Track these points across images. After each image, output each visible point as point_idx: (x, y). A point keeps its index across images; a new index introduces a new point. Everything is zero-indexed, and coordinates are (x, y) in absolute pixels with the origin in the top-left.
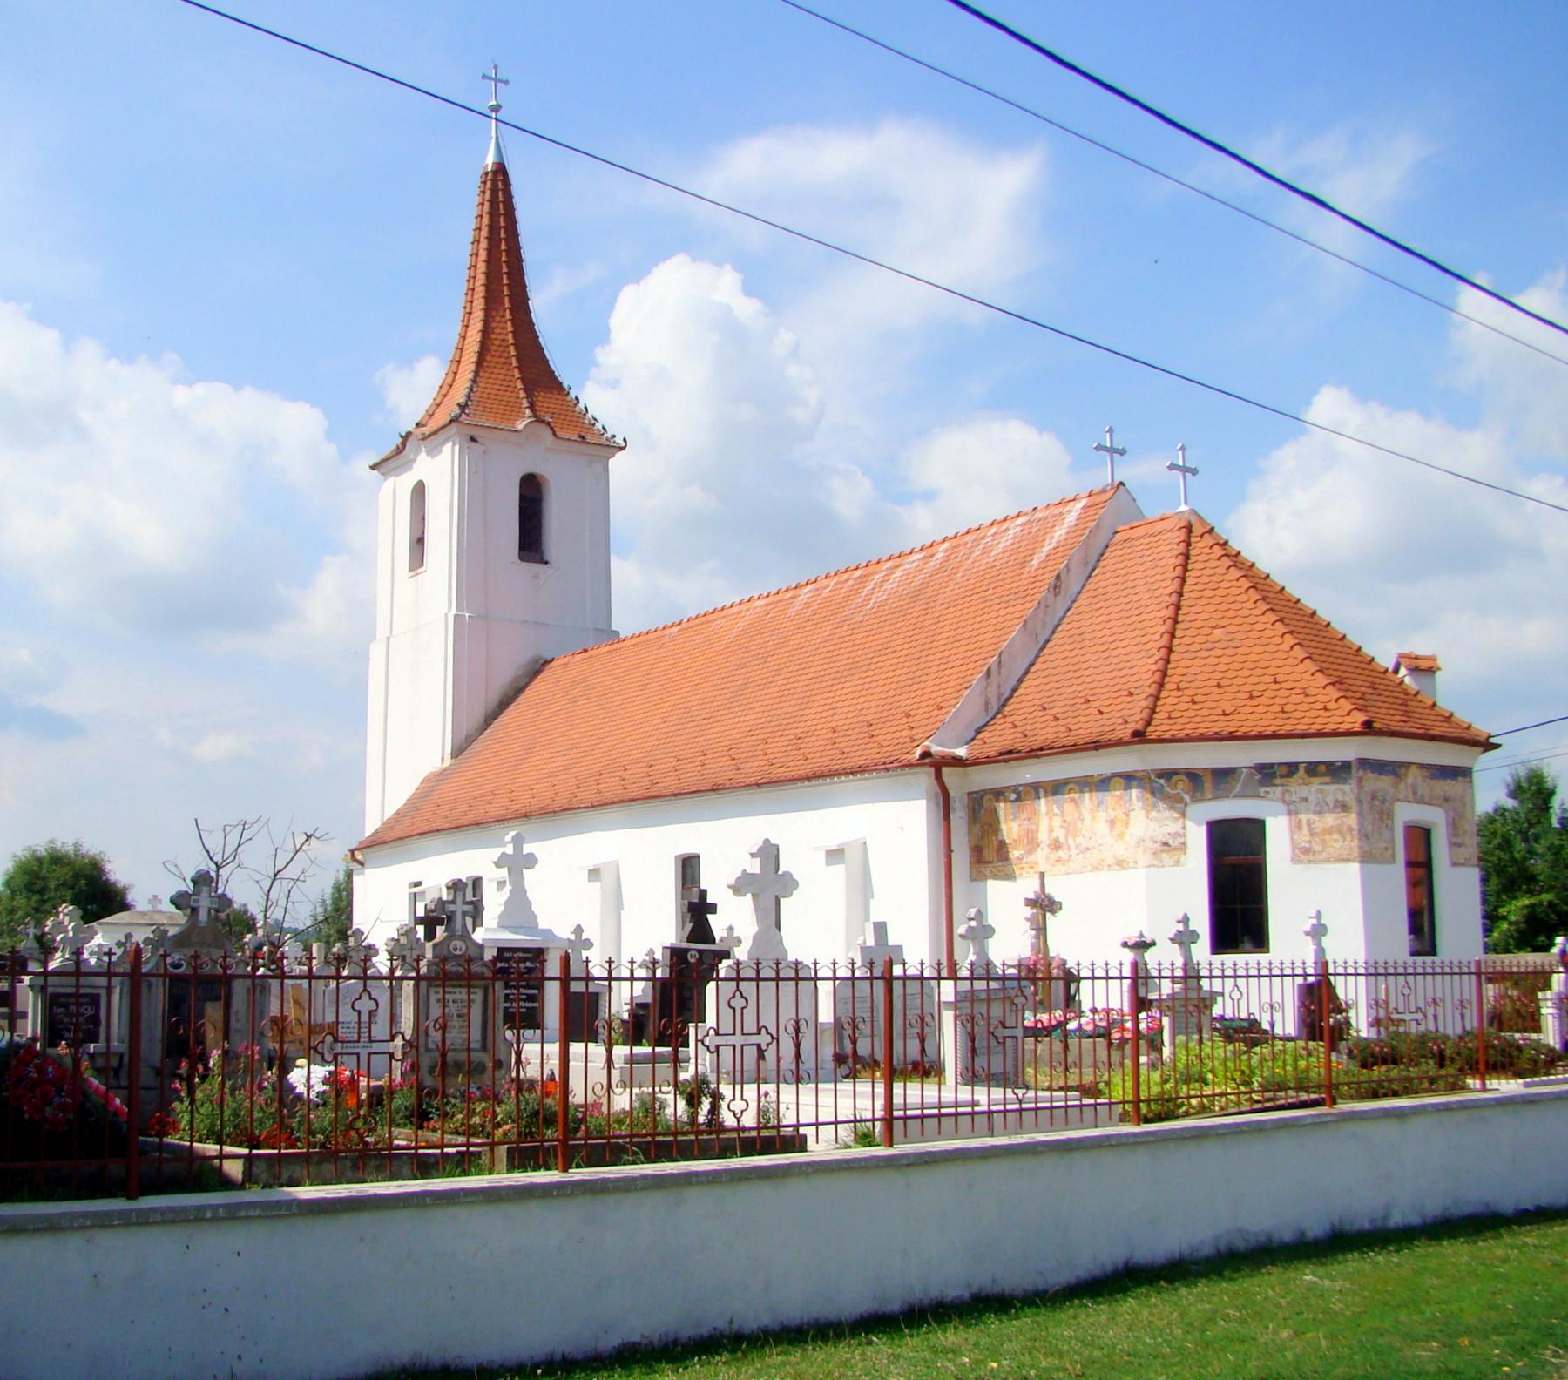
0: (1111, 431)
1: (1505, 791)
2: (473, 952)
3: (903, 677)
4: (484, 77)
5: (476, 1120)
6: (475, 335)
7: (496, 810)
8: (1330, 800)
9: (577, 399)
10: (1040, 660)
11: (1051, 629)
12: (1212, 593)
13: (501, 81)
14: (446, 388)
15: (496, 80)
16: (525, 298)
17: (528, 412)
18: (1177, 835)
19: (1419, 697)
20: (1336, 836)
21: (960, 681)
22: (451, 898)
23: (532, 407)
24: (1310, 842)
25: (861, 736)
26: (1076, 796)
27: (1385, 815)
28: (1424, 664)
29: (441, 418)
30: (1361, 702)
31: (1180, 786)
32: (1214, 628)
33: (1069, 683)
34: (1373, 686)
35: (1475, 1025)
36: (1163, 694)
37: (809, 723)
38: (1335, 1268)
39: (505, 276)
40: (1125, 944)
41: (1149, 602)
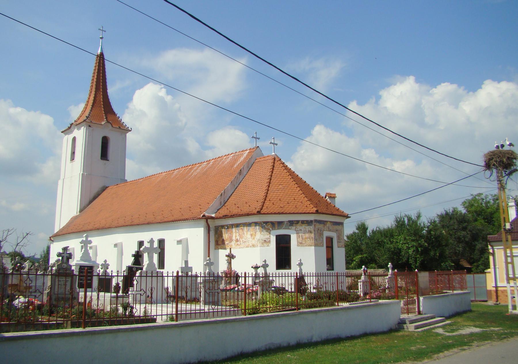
0: (256, 133)
1: (355, 228)
2: (69, 267)
3: (199, 195)
4: (99, 29)
5: (66, 314)
6: (92, 98)
7: (90, 227)
8: (307, 230)
9: (119, 117)
10: (235, 192)
11: (238, 184)
12: (280, 176)
13: (104, 31)
14: (83, 112)
15: (102, 30)
16: (107, 89)
17: (105, 119)
18: (268, 238)
19: (331, 204)
20: (308, 240)
21: (214, 197)
22: (63, 252)
23: (106, 118)
24: (302, 241)
25: (188, 210)
26: (243, 228)
27: (321, 234)
28: (332, 196)
29: (82, 120)
30: (316, 205)
31: (269, 226)
32: (279, 185)
33: (242, 198)
34: (319, 201)
35: (336, 289)
36: (266, 202)
37: (174, 206)
38: (296, 353)
39: (101, 83)
40: (252, 267)
41: (263, 178)
